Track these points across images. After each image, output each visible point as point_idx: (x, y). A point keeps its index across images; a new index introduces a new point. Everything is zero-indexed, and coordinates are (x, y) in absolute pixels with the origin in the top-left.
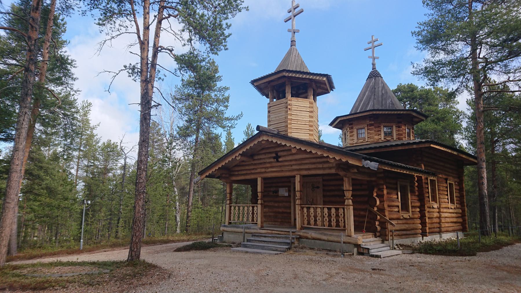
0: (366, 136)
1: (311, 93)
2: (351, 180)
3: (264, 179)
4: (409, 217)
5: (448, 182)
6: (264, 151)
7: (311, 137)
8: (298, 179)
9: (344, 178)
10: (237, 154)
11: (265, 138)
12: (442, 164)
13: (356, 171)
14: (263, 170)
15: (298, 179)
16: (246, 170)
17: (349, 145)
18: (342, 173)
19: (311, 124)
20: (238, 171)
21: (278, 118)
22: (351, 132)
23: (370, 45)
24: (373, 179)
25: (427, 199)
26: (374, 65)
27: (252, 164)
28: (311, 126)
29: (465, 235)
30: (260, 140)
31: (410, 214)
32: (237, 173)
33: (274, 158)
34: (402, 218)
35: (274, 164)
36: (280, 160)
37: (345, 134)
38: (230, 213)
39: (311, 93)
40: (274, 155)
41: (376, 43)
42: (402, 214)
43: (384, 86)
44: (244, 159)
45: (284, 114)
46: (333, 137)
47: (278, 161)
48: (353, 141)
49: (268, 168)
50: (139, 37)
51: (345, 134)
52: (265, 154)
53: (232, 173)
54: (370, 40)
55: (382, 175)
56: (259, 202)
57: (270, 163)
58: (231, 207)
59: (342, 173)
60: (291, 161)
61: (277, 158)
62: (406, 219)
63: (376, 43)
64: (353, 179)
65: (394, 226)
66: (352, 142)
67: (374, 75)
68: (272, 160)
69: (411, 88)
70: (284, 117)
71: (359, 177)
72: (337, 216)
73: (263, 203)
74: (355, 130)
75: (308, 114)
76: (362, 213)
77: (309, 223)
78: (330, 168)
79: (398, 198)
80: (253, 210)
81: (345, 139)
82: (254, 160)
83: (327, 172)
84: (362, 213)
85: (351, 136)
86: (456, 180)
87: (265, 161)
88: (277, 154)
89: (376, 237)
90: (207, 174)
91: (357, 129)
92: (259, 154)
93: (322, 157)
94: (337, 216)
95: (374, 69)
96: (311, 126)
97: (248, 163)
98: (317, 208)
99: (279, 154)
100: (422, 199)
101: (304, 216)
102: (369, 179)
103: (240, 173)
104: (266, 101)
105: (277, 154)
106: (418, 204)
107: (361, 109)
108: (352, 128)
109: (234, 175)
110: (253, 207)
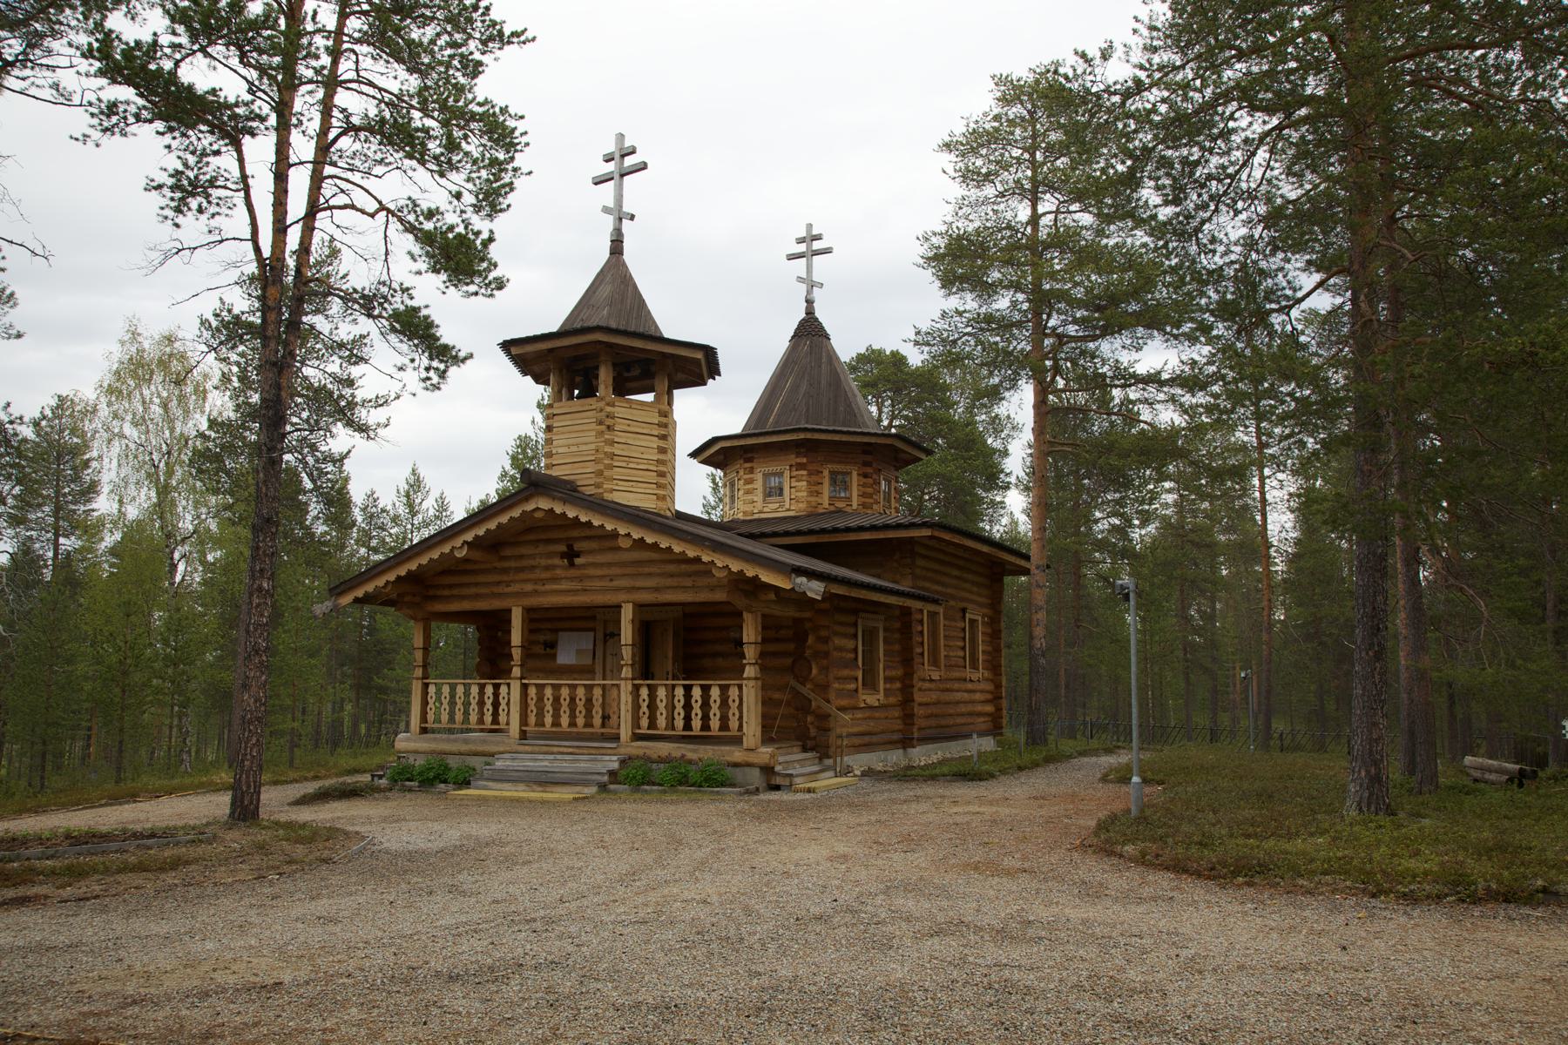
0: (788, 496)
3: (529, 612)
7: (660, 504)
8: (627, 613)
9: (745, 615)
10: (458, 542)
11: (544, 504)
12: (956, 572)
13: (772, 596)
14: (529, 587)
15: (627, 613)
16: (476, 584)
17: (740, 516)
18: (740, 602)
19: (662, 468)
20: (451, 586)
21: (574, 449)
22: (750, 482)
23: (802, 248)
24: (807, 615)
25: (917, 659)
27: (494, 570)
29: (999, 744)
30: (530, 507)
31: (881, 696)
32: (446, 592)
33: (563, 555)
36: (578, 561)
37: (732, 485)
38: (425, 703)
40: (563, 548)
43: (832, 356)
44: (477, 555)
45: (593, 439)
46: (694, 490)
47: (572, 565)
48: (754, 504)
49: (544, 581)
50: (257, 250)
51: (732, 485)
53: (431, 593)
54: (803, 234)
56: (750, 671)
57: (547, 568)
58: (426, 686)
60: (609, 565)
61: (571, 555)
62: (871, 708)
63: (817, 245)
64: (764, 616)
65: (845, 723)
66: (748, 508)
67: (810, 332)
68: (557, 561)
69: (898, 360)
70: (593, 446)
71: (777, 610)
72: (724, 703)
74: (759, 477)
75: (655, 443)
76: (777, 696)
77: (652, 725)
78: (712, 589)
79: (856, 659)
80: (496, 695)
81: (732, 497)
83: (703, 597)
84: (777, 696)
85: (748, 492)
86: (985, 611)
87: (532, 562)
88: (570, 547)
89: (805, 749)
90: (360, 593)
91: (766, 476)
93: (698, 560)
94: (724, 703)
95: (810, 312)
97: (483, 566)
98: (674, 687)
99: (577, 546)
100: (907, 660)
101: (674, 707)
102: (797, 615)
103: (455, 592)
104: (539, 392)
105: (570, 547)
106: (899, 673)
107: (776, 423)
108: (751, 470)
109: (435, 598)
110: (496, 687)
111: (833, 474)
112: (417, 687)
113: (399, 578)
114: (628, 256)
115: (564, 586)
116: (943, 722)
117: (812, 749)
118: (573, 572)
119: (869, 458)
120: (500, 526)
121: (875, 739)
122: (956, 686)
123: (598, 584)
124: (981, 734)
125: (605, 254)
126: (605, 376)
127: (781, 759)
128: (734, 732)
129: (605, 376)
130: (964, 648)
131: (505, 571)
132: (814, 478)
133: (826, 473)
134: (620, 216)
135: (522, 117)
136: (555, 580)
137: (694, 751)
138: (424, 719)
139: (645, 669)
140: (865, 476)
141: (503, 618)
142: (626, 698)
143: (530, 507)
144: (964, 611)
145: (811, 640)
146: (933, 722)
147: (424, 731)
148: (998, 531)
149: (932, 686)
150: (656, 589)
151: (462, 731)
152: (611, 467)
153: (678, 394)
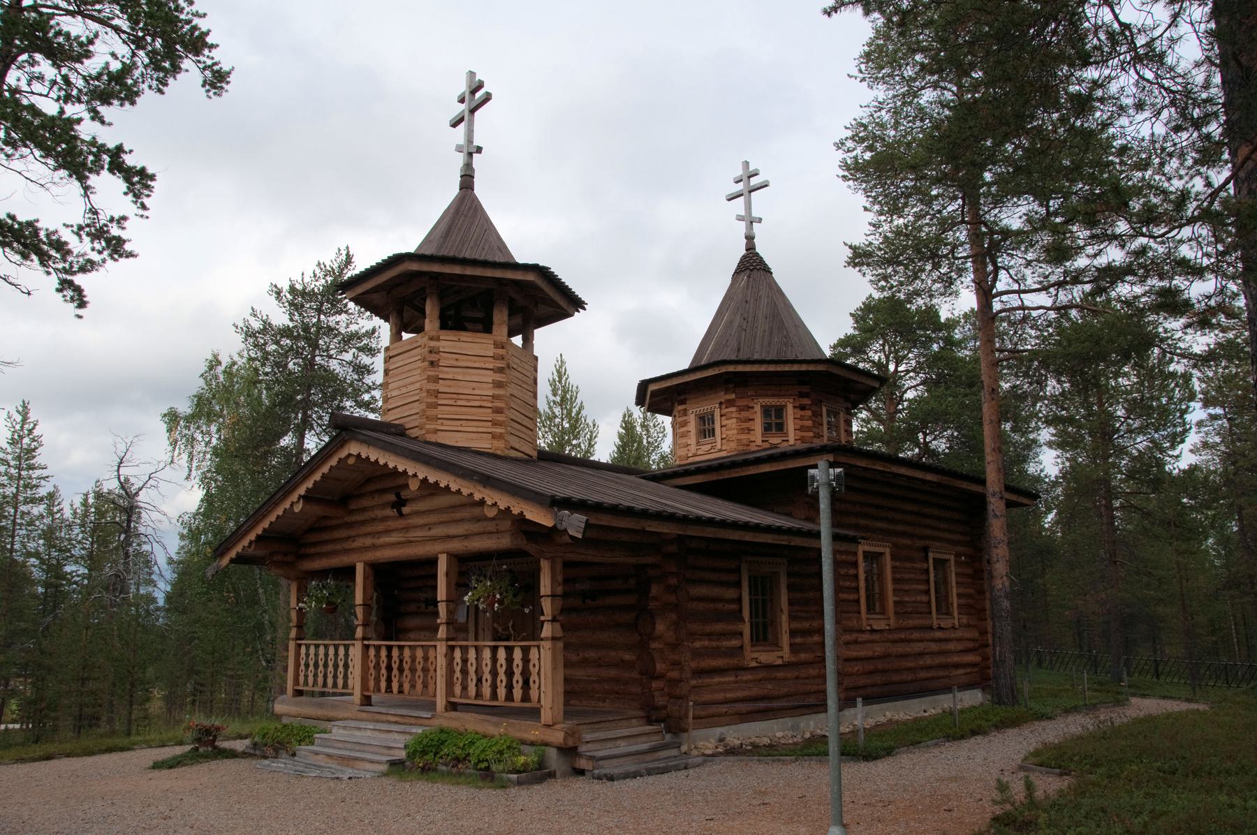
0: (733, 433)
1: (500, 317)
2: (559, 567)
4: (779, 662)
5: (931, 555)
6: (371, 488)
14: (368, 541)
18: (532, 548)
19: (498, 404)
21: (404, 390)
23: (740, 186)
26: (750, 238)
28: (498, 411)
30: (343, 454)
34: (754, 664)
35: (392, 524)
36: (405, 510)
39: (500, 317)
40: (393, 498)
41: (754, 181)
42: (754, 655)
44: (317, 510)
52: (372, 494)
55: (673, 548)
56: (547, 631)
59: (532, 548)
63: (754, 181)
64: (567, 565)
67: (752, 266)
70: (418, 386)
73: (560, 634)
75: (490, 377)
79: (740, 611)
82: (351, 512)
88: (398, 495)
89: (650, 722)
92: (360, 496)
95: (750, 247)
96: (498, 411)
97: (334, 522)
102: (632, 560)
105: (398, 495)
111: (766, 411)
112: (292, 645)
113: (259, 537)
114: (480, 191)
115: (394, 538)
116: (896, 678)
117: (658, 721)
118: (401, 523)
119: (806, 389)
120: (324, 476)
121: (775, 704)
122: (916, 635)
123: (419, 533)
124: (964, 687)
125: (454, 190)
126: (431, 308)
127: (588, 737)
128: (534, 704)
129: (431, 308)
130: (927, 592)
131: (350, 525)
132: (745, 414)
133: (758, 408)
134: (471, 151)
135: (205, 15)
136: (388, 532)
137: (497, 725)
138: (296, 682)
139: (458, 631)
140: (803, 408)
141: (349, 572)
142: (441, 662)
143: (343, 454)
144: (925, 550)
145: (655, 590)
146: (878, 679)
147: (299, 693)
148: (1032, 469)
149: (876, 637)
150: (466, 536)
151: (343, 694)
152: (436, 405)
153: (540, 334)
